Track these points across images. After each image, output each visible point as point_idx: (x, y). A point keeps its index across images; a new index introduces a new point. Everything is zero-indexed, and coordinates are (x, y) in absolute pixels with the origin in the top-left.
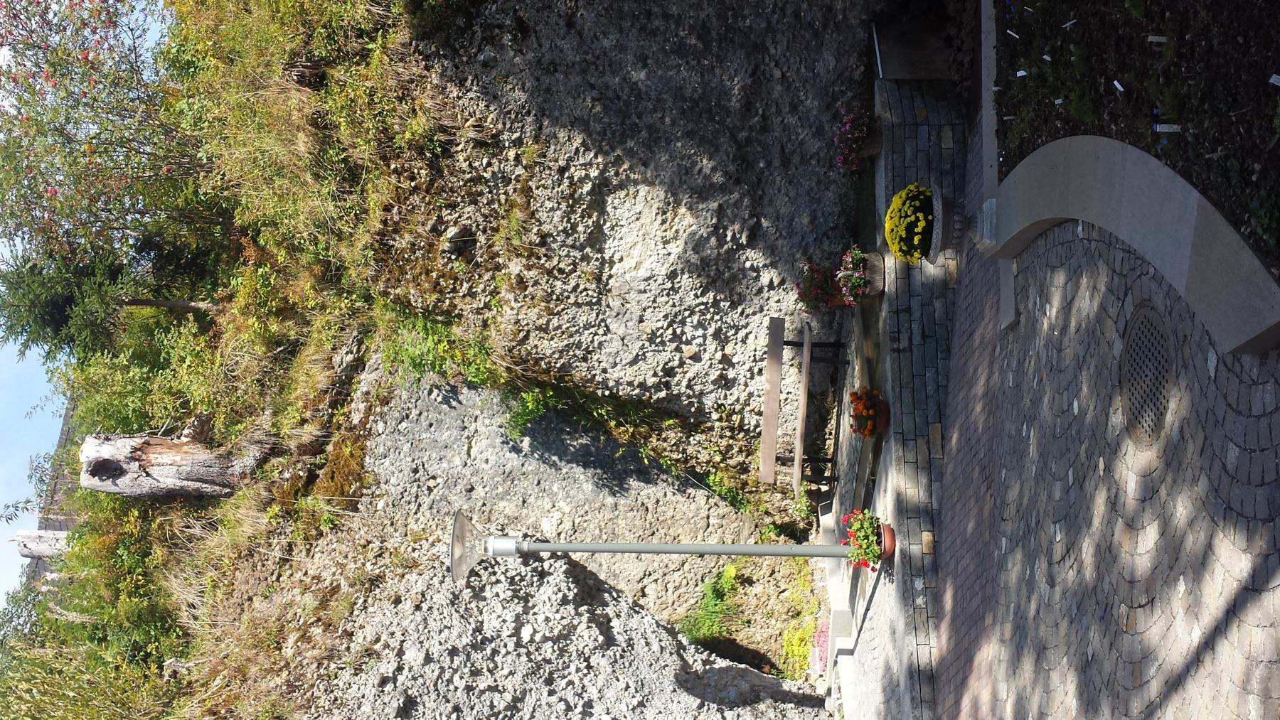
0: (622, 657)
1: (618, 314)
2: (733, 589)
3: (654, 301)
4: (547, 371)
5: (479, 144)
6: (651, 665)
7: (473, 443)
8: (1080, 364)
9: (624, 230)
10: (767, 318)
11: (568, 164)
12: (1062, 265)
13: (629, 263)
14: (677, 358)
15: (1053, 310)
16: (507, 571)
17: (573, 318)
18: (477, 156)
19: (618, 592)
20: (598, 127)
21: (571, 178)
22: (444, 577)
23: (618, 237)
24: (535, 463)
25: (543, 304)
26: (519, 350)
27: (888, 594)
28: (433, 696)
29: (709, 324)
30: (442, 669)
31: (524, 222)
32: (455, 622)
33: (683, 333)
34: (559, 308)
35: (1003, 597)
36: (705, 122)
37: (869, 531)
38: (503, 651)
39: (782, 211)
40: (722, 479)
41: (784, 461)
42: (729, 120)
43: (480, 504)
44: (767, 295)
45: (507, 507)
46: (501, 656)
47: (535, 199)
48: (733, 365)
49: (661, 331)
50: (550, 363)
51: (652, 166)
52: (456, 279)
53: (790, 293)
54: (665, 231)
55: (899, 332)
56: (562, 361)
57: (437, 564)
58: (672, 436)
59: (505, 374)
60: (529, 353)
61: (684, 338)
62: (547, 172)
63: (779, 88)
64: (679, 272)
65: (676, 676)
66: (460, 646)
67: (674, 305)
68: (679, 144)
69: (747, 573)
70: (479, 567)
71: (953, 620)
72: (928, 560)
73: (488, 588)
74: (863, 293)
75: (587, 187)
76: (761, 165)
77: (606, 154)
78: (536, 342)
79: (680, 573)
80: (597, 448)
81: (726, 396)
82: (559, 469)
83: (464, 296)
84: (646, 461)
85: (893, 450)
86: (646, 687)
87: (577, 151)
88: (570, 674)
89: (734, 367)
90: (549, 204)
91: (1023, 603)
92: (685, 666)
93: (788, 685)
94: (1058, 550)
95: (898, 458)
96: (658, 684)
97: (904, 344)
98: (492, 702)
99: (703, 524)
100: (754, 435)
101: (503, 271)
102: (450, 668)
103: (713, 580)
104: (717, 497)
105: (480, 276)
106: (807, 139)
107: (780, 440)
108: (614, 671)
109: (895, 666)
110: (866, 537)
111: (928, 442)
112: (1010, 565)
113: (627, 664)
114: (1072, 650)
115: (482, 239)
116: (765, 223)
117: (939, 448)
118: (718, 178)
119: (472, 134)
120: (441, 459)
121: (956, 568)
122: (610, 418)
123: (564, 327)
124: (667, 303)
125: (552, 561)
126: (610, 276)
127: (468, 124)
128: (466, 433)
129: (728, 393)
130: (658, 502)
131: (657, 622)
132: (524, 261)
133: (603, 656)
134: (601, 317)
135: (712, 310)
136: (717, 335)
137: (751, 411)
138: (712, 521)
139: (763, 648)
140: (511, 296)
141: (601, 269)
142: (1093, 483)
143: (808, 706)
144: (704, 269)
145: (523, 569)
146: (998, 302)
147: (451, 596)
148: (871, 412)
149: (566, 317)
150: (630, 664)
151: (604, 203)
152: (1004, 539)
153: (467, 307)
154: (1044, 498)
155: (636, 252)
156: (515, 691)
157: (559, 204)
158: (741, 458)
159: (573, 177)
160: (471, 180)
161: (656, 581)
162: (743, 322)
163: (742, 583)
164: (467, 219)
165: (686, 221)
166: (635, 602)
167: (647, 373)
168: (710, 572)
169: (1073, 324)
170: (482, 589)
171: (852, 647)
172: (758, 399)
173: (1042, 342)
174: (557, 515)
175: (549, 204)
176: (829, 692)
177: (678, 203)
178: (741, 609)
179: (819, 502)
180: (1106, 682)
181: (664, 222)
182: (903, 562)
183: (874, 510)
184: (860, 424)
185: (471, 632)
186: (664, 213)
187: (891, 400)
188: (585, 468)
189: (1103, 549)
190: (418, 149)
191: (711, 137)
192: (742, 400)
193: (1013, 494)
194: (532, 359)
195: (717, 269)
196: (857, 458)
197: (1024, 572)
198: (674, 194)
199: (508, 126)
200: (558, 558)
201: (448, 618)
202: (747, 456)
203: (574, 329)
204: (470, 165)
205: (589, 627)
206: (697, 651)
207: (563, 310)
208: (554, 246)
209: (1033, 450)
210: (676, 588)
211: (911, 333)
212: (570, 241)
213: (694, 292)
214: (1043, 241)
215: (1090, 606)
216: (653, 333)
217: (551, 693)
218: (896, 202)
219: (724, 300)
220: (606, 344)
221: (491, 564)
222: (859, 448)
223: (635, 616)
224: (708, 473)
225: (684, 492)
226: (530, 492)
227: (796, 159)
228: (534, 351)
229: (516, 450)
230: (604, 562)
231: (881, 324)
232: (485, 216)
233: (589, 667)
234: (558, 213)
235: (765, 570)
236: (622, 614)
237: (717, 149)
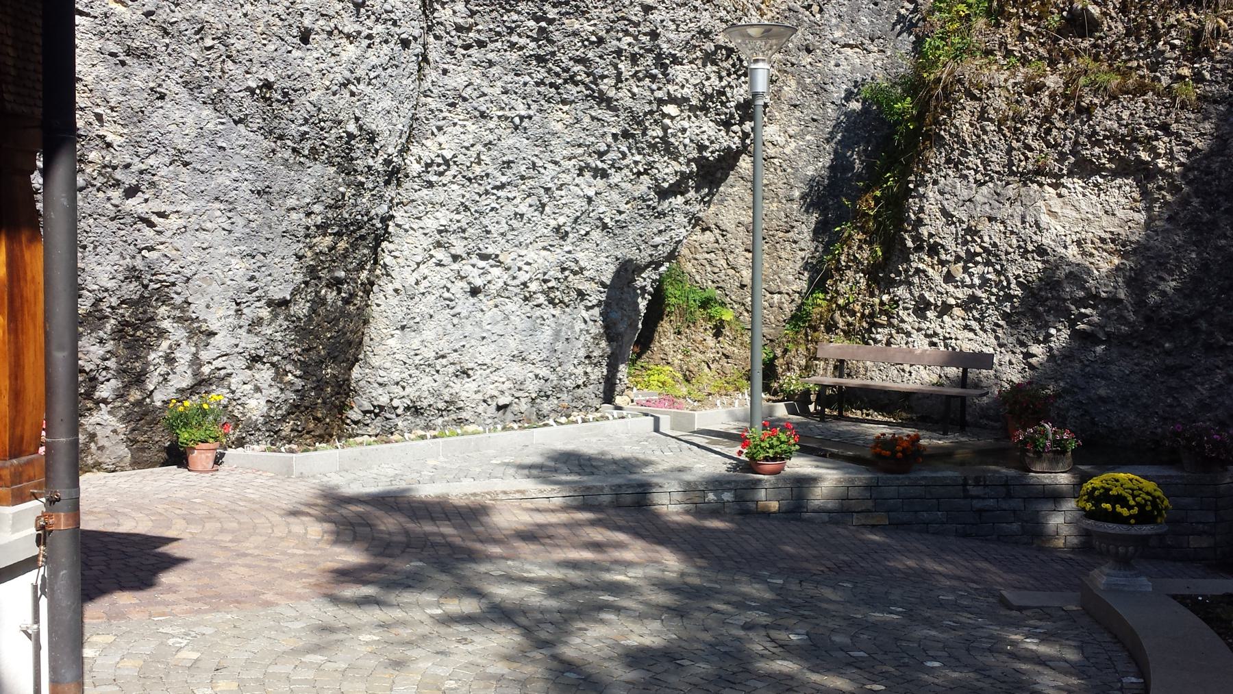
0: (649, 206)
1: (998, 194)
2: (711, 318)
3: (1012, 232)
4: (936, 122)
5: (1197, 34)
6: (641, 236)
7: (857, 50)
8: (982, 671)
9: (1094, 198)
10: (992, 351)
11: (1173, 134)
12: (1087, 658)
13: (1056, 204)
14: (948, 257)
15: (1032, 644)
16: (731, 87)
17: (994, 147)
18: (1183, 33)
19: (709, 202)
20: (1215, 166)
21: (1157, 138)
22: (727, 21)
23: (1087, 192)
24: (834, 115)
25: (1011, 113)
26: (959, 91)
27: (711, 465)
28: (612, 16)
29: (986, 291)
30: (637, 25)
31: (1105, 88)
32: (682, 35)
33: (976, 264)
34: (1006, 131)
35: (724, 578)
36: (1220, 283)
37: (778, 450)
38: (654, 86)
39: (1112, 367)
40: (819, 305)
41: (840, 367)
42: (1221, 309)
43: (793, 61)
44: (1018, 351)
45: (790, 89)
46: (650, 84)
47: (1133, 100)
48: (940, 316)
49: (979, 241)
50: (945, 124)
51: (1168, 226)
52: (1040, 18)
53: (1019, 376)
54: (1093, 243)
55: (985, 486)
56: (947, 137)
57: (739, 13)
58: (864, 255)
59: (932, 77)
60: (956, 101)
61: (971, 265)
62: (1163, 112)
64: (1045, 258)
65: (631, 260)
66: (659, 42)
67: (1007, 253)
68: (1194, 256)
69: (726, 331)
70: (735, 58)
71: (695, 528)
72: (752, 505)
73: (715, 68)
74: (1028, 451)
75: (1144, 156)
76: (1167, 345)
77: (1183, 175)
78: (968, 108)
79: (725, 266)
80: (850, 179)
81: (907, 309)
82: (828, 141)
83: (1020, 28)
84: (838, 229)
85: (862, 477)
86: (621, 232)
87: (1188, 143)
88: (633, 155)
89: (938, 317)
90: (1125, 115)
91: (722, 597)
92: (640, 269)
93: (623, 368)
94: (781, 636)
95: (852, 480)
96: (623, 242)
97: (973, 490)
98: (606, 77)
99: (773, 287)
100: (865, 337)
101: (1048, 69)
102: (639, 31)
103: (718, 298)
104: (800, 301)
106: (1197, 393)
107: (861, 364)
108: (635, 199)
109: (649, 470)
110: (772, 447)
111: (869, 511)
112: (757, 586)
113: (641, 212)
114: (683, 644)
115: (1086, 44)
116: (1100, 349)
117: (863, 522)
118: (1153, 298)
119: (1209, 26)
120: (840, 16)
121: (747, 533)
122: (883, 191)
123: (985, 137)
124: (1010, 246)
125: (740, 134)
126: (1041, 185)
127: (1221, 22)
128: (867, 42)
129: (911, 311)
130: (795, 242)
131: (681, 241)
132: (1061, 90)
133: (649, 188)
134: (995, 176)
135: (1001, 293)
136: (974, 299)
137: (891, 335)
138: (776, 297)
139: (655, 347)
140: (1020, 78)
141: (1051, 174)
142: (856, 676)
143: (605, 388)
144: (1048, 284)
145: (733, 104)
146: (1025, 588)
147: (707, 30)
148: (900, 454)
149: (995, 139)
150: (641, 215)
151: (1127, 176)
152: (781, 581)
153: (1008, 31)
154: (831, 625)
155: (1069, 211)
156: (617, 100)
157: (1126, 126)
158: (841, 324)
159: (1157, 139)
160: (1155, 27)
161: (717, 242)
162: (987, 326)
163: (715, 326)
164: (1110, 27)
165: (1104, 264)
166: (700, 219)
167: (933, 226)
168: (727, 295)
169: (1024, 667)
170: (714, 63)
172: (903, 342)
173: (995, 633)
174: (781, 140)
175: (1125, 115)
176: (619, 408)
177: (1124, 255)
178: (691, 325)
179: (799, 402)
180: (658, 677)
181: (1103, 240)
182: (748, 481)
183: (799, 456)
184: (880, 441)
185: (673, 52)
186: (1113, 241)
187: (912, 475)
188: (829, 167)
189: (788, 682)
191: (1202, 289)
192: (904, 326)
193: (828, 593)
194: (950, 105)
195: (1047, 299)
196: (849, 441)
197: (753, 599)
198: (1134, 250)
199: (1218, 65)
200: (743, 140)
201: (686, 28)
203: (982, 148)
204: (1172, 26)
205: (676, 172)
206: (654, 281)
207: (1004, 136)
208: (1077, 123)
209: (878, 616)
210: (710, 262)
211: (984, 498)
212: (1082, 139)
213: (1022, 274)
214: (1109, 639)
215: (730, 665)
216: (976, 232)
217: (615, 136)
218: (1150, 486)
219: (1013, 307)
220: (965, 183)
221: (738, 70)
222: (857, 442)
223: (686, 220)
224: (825, 292)
225: (805, 269)
226: (805, 111)
227: (1173, 382)
228: (958, 107)
229: (849, 96)
230: (735, 189)
231: (993, 467)
232: (1112, 45)
233: (639, 174)
234: (1116, 126)
235: (729, 349)
236: (688, 207)
237: (1186, 297)
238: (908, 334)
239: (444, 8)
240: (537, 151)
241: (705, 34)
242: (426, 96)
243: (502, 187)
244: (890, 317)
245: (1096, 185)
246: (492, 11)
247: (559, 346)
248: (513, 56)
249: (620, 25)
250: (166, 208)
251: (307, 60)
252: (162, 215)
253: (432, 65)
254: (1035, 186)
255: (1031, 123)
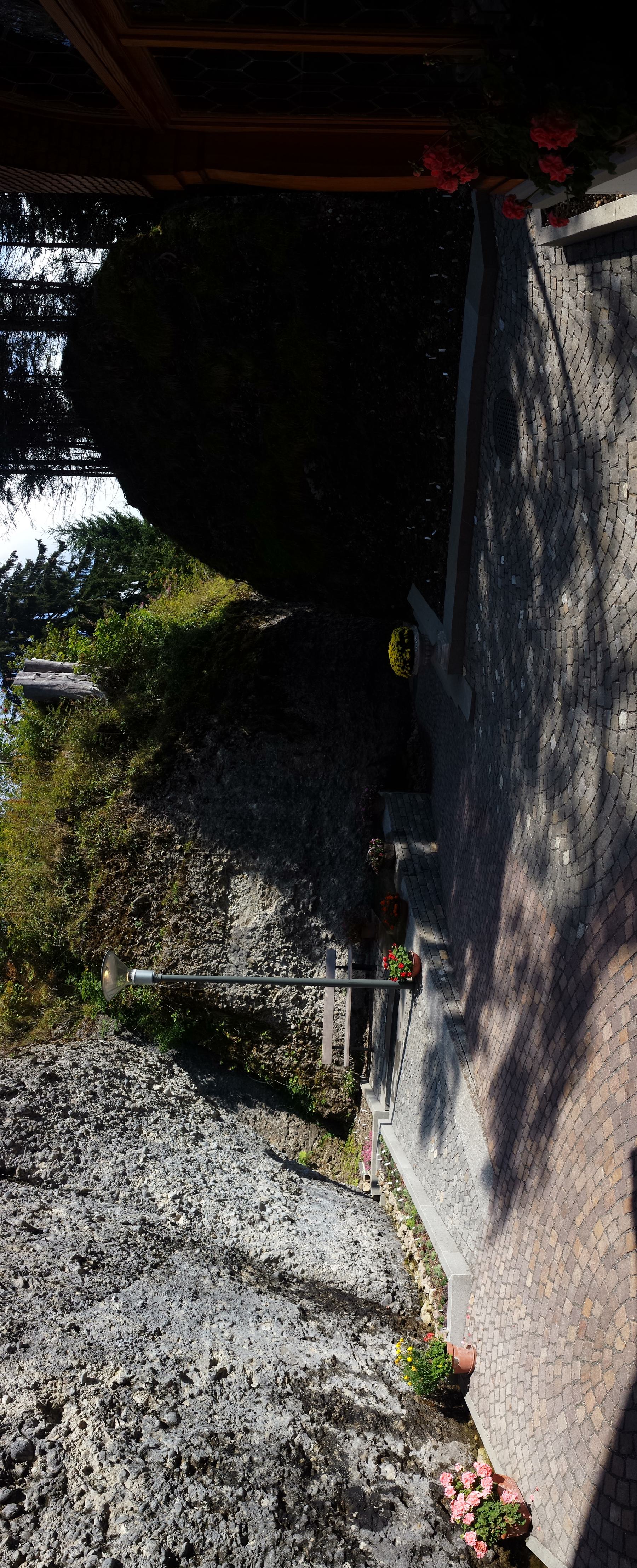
3: (257, 944)
13: (242, 920)
21: (211, 862)
23: (236, 903)
33: (274, 967)
63: (327, 819)
67: (268, 947)
75: (220, 869)
77: (232, 850)
90: (196, 877)
99: (285, 1132)
105: (151, 931)
118: (295, 868)
126: (231, 927)
130: (255, 1118)
138: (291, 1130)
155: (247, 913)
175: (196, 877)
181: (263, 895)
186: (264, 889)
190: (123, 850)
202: (314, 1060)
208: (198, 905)
212: (207, 901)
224: (288, 1078)
238: (316, 1011)
239: (39, 1168)
242: (117, 1199)
244: (304, 1024)
245: (233, 898)
246: (49, 1136)
250: (206, 1358)
252: (213, 1362)
253: (89, 1188)
254: (232, 931)
255: (195, 930)
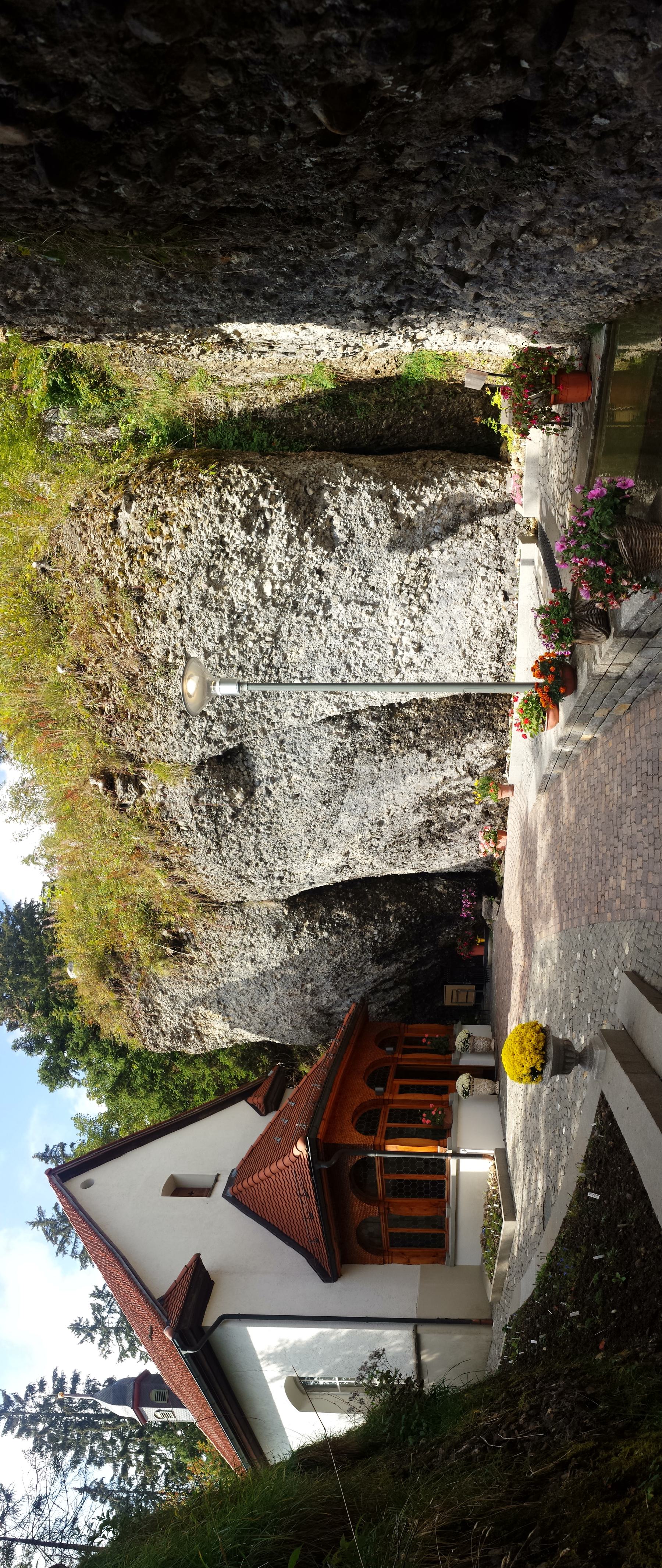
30: (220, 655)
32: (213, 619)
38: (255, 613)
171: (210, 1186)
240: (321, 656)
241: (204, 600)
243: (348, 667)
247: (460, 569)
248: (269, 704)
249: (225, 663)
251: (308, 793)
